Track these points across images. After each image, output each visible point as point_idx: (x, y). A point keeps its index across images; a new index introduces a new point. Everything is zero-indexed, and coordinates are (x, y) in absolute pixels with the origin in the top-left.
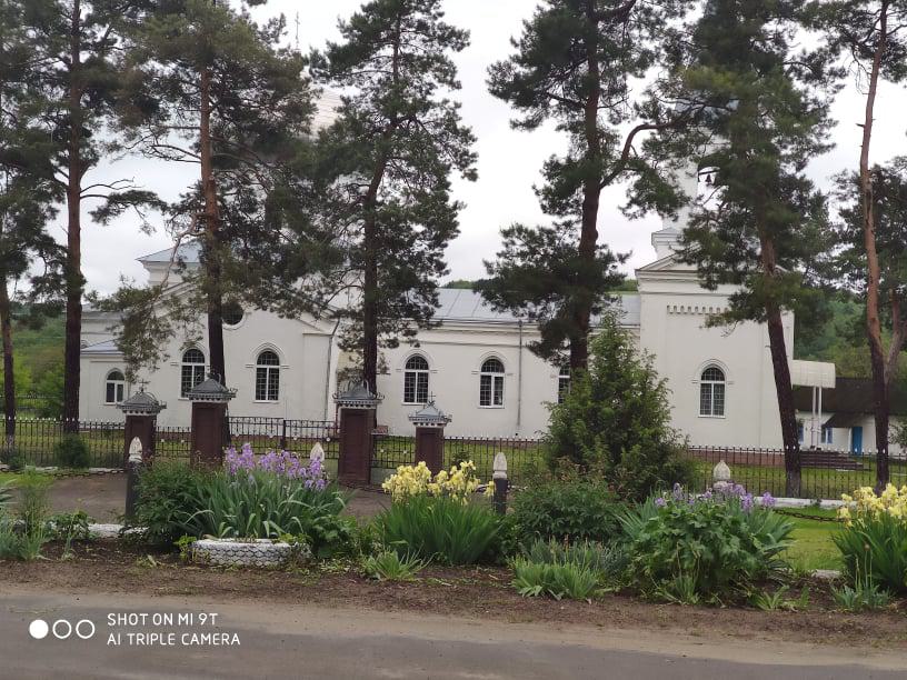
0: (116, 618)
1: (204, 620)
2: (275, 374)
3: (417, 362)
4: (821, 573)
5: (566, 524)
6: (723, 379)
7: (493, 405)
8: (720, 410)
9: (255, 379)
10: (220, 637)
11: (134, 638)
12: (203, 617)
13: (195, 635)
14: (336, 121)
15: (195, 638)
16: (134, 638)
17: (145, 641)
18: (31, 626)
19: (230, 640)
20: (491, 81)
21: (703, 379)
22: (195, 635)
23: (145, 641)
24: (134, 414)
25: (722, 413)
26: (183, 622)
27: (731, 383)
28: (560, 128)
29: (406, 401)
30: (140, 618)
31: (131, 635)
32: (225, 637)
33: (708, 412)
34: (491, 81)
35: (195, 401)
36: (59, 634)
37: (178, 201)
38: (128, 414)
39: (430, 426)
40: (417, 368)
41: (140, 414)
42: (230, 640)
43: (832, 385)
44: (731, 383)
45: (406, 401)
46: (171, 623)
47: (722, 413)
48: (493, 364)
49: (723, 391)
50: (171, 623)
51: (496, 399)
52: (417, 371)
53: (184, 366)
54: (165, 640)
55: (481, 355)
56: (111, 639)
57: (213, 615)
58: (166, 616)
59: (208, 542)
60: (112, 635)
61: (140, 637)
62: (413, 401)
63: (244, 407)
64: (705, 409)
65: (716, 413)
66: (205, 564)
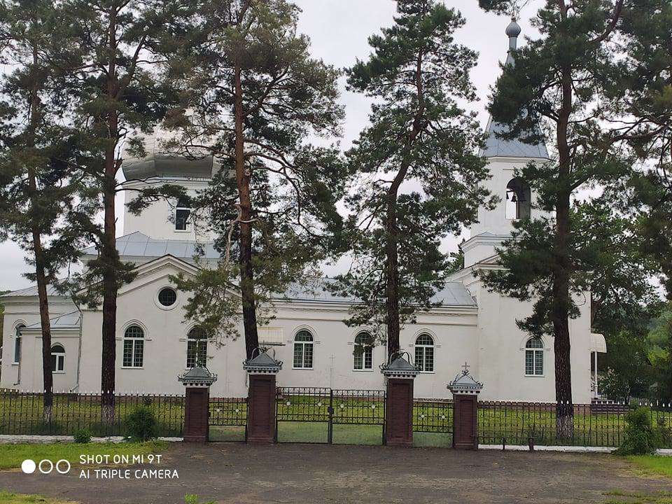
2: (140, 345)
3: (425, 339)
6: (432, 343)
7: (133, 367)
10: (164, 472)
13: (145, 471)
17: (108, 475)
19: (171, 475)
21: (527, 347)
22: (145, 471)
23: (108, 475)
24: (194, 386)
25: (432, 370)
27: (439, 346)
29: (295, 366)
32: (168, 472)
33: (531, 373)
35: (253, 373)
37: (366, 54)
38: (189, 386)
39: (469, 393)
40: (424, 344)
41: (199, 386)
42: (171, 475)
43: (604, 350)
44: (439, 346)
45: (295, 366)
47: (432, 370)
48: (424, 339)
49: (542, 356)
51: (136, 360)
52: (304, 343)
53: (189, 342)
54: (123, 475)
55: (295, 327)
56: (83, 474)
58: (123, 457)
59: (663, 451)
60: (83, 471)
62: (130, 365)
63: (290, 378)
64: (529, 371)
65: (427, 370)
66: (659, 457)
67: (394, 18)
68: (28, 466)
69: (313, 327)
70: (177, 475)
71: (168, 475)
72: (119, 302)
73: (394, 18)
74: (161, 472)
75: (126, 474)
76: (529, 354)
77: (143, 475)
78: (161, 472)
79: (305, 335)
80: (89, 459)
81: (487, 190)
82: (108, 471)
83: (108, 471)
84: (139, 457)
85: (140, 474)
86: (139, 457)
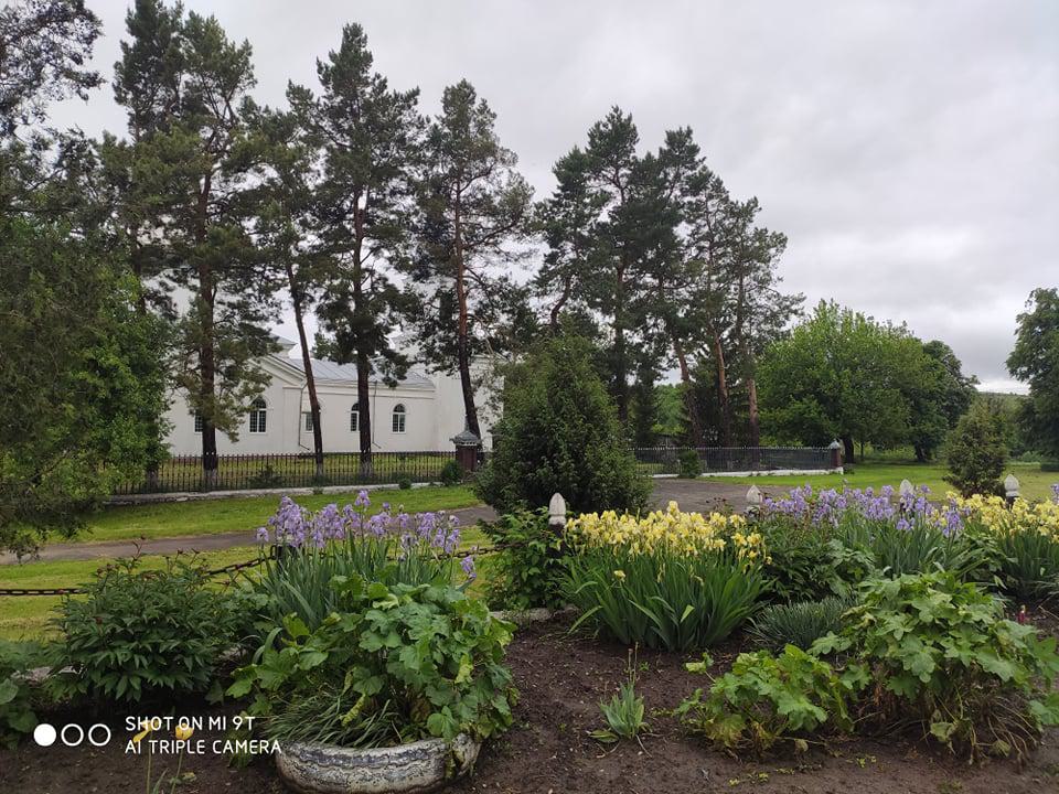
0: (136, 722)
1: (239, 724)
4: (754, 657)
5: (157, 604)
8: (263, 429)
9: (413, 451)
11: (157, 745)
12: (237, 721)
14: (558, 174)
15: (228, 745)
16: (157, 745)
17: (169, 748)
18: (37, 730)
20: (116, 85)
22: (228, 742)
23: (169, 748)
25: (264, 431)
26: (215, 727)
28: (129, 114)
30: (164, 722)
31: (154, 742)
33: (255, 431)
34: (116, 85)
36: (70, 742)
46: (200, 727)
50: (200, 727)
57: (168, 718)
58: (194, 719)
61: (164, 744)
64: (395, 429)
65: (260, 431)
67: (290, 83)
68: (45, 735)
69: (404, 402)
70: (278, 748)
71: (265, 748)
72: (303, 321)
73: (290, 83)
74: (253, 744)
75: (199, 747)
76: (395, 417)
77: (226, 748)
78: (253, 744)
79: (399, 408)
80: (140, 723)
81: (596, 134)
82: (170, 743)
83: (170, 743)
84: (218, 719)
85: (220, 747)
86: (218, 719)
